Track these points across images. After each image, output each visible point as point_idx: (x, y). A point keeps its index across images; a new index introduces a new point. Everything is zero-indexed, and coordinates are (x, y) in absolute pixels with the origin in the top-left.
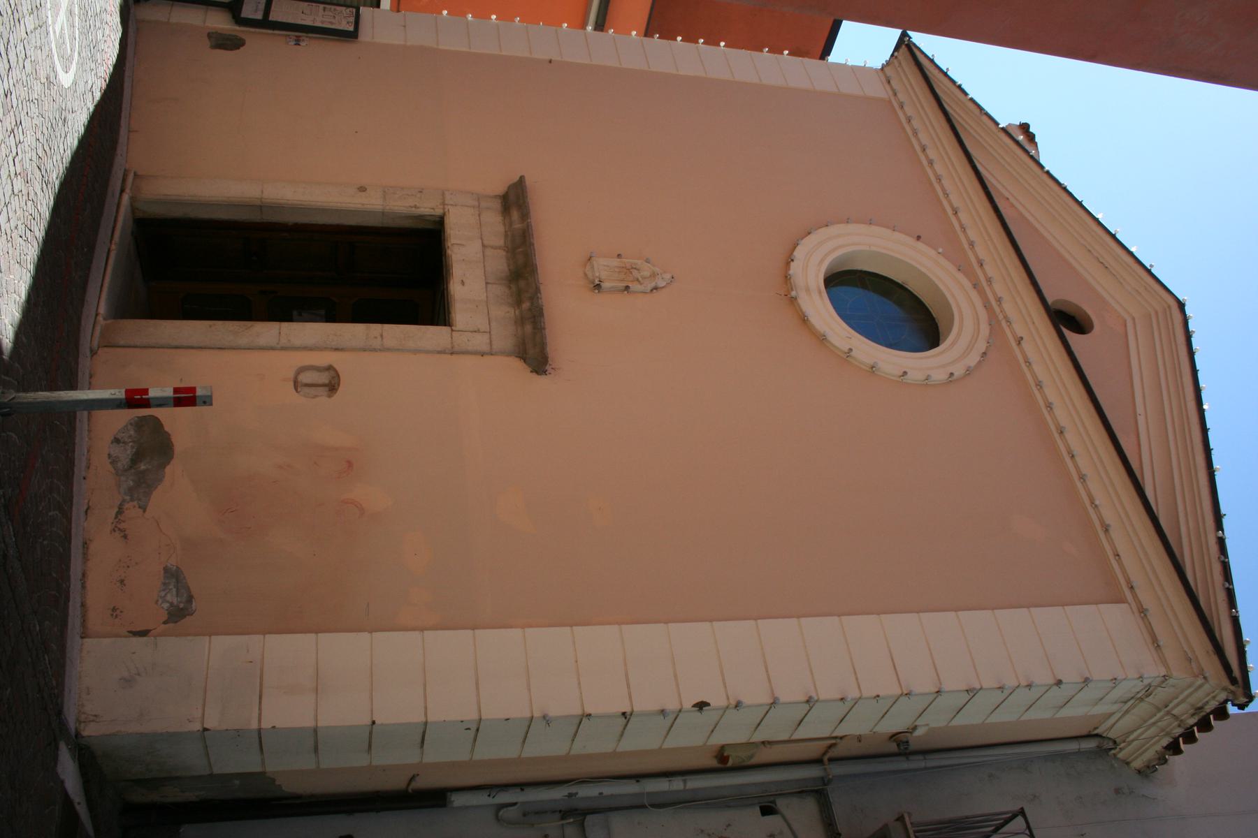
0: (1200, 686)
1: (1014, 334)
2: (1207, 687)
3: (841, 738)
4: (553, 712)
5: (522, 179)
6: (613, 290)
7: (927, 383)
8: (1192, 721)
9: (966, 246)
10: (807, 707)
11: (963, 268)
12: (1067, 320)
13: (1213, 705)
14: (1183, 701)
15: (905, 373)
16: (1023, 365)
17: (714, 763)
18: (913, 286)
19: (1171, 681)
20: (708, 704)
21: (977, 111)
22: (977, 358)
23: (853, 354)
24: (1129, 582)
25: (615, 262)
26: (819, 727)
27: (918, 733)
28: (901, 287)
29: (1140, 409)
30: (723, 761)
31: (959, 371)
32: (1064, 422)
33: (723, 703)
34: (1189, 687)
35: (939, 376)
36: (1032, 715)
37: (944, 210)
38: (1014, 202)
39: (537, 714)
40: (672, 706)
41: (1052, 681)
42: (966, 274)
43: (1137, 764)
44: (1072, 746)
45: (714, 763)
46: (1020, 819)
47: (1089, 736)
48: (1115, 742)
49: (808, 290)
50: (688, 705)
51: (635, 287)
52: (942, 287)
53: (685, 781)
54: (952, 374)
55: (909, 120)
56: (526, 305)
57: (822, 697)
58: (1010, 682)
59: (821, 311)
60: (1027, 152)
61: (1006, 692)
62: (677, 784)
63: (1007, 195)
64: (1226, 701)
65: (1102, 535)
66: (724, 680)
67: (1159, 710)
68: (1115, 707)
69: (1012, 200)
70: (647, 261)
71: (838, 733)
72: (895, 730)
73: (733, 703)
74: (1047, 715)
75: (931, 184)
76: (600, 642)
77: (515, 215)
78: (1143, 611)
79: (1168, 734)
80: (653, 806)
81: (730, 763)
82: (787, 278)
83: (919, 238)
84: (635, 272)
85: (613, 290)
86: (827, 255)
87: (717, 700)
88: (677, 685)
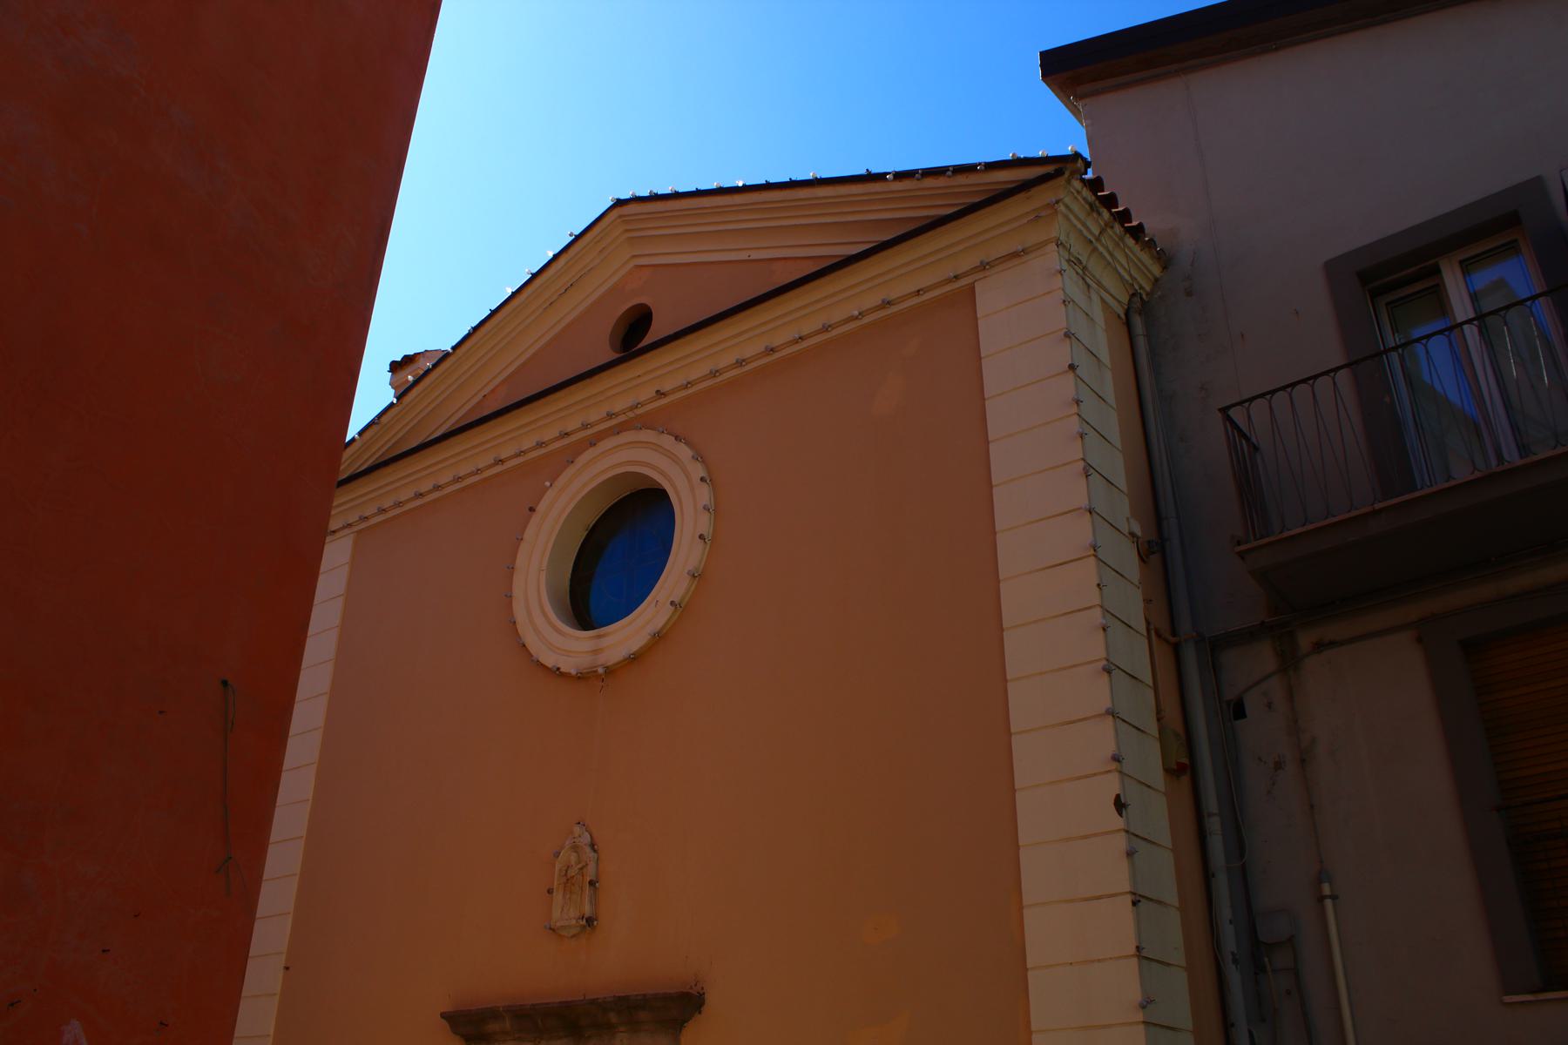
0: (1067, 206)
1: (651, 400)
2: (1067, 200)
3: (1148, 623)
4: (1136, 995)
5: (443, 1015)
6: (595, 902)
7: (715, 510)
8: (1106, 214)
9: (543, 451)
10: (1116, 672)
11: (570, 455)
12: (634, 334)
13: (1086, 193)
14: (1084, 224)
15: (701, 537)
16: (690, 391)
17: (1185, 779)
18: (591, 520)
19: (1063, 238)
20: (1118, 797)
21: (375, 428)
22: (682, 446)
23: (677, 601)
24: (949, 281)
25: (558, 897)
26: (1137, 655)
27: (1137, 530)
28: (593, 532)
29: (743, 256)
30: (1182, 769)
31: (698, 471)
32: (759, 347)
33: (1115, 777)
34: (1068, 219)
35: (704, 495)
36: (1109, 392)
37: (497, 475)
38: (490, 387)
39: (1140, 1017)
40: (1121, 842)
41: (1071, 375)
42: (579, 453)
43: (1156, 270)
44: (1141, 342)
45: (1185, 779)
46: (1231, 412)
47: (1128, 324)
48: (1133, 295)
49: (596, 652)
50: (1119, 822)
51: (590, 873)
52: (594, 484)
53: (1210, 815)
54: (702, 479)
55: (382, 511)
56: (613, 1017)
57: (1103, 654)
58: (1075, 425)
59: (624, 636)
60: (428, 372)
61: (1087, 429)
62: (1214, 825)
63: (480, 396)
64: (1083, 180)
65: (894, 309)
66: (1087, 777)
67: (1095, 249)
68: (1095, 297)
69: (486, 391)
70: (557, 855)
71: (1142, 628)
72: (1136, 559)
73: (1114, 765)
74: (1108, 375)
75: (463, 489)
76: (1047, 934)
77: (493, 1027)
78: (983, 267)
79: (1122, 239)
80: (1242, 855)
81: (1185, 760)
82: (581, 677)
83: (532, 510)
84: (571, 873)
85: (595, 902)
86: (550, 623)
87: (1112, 785)
88: (1095, 835)
